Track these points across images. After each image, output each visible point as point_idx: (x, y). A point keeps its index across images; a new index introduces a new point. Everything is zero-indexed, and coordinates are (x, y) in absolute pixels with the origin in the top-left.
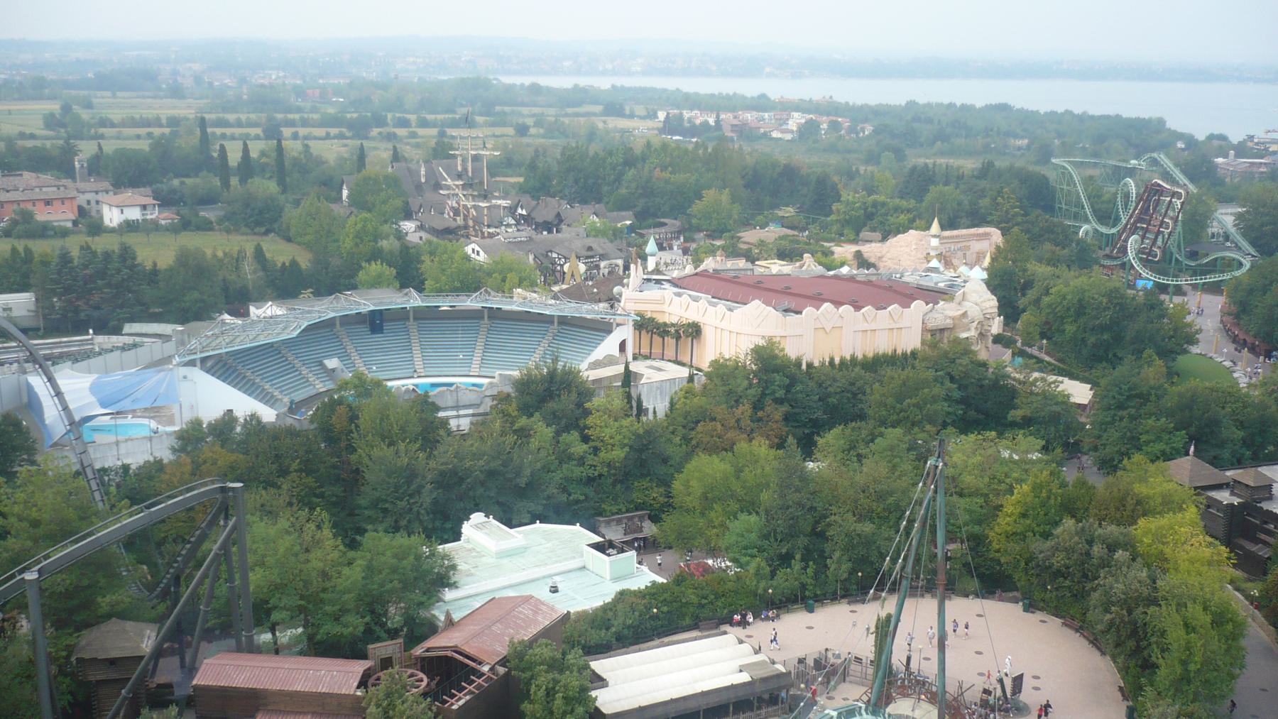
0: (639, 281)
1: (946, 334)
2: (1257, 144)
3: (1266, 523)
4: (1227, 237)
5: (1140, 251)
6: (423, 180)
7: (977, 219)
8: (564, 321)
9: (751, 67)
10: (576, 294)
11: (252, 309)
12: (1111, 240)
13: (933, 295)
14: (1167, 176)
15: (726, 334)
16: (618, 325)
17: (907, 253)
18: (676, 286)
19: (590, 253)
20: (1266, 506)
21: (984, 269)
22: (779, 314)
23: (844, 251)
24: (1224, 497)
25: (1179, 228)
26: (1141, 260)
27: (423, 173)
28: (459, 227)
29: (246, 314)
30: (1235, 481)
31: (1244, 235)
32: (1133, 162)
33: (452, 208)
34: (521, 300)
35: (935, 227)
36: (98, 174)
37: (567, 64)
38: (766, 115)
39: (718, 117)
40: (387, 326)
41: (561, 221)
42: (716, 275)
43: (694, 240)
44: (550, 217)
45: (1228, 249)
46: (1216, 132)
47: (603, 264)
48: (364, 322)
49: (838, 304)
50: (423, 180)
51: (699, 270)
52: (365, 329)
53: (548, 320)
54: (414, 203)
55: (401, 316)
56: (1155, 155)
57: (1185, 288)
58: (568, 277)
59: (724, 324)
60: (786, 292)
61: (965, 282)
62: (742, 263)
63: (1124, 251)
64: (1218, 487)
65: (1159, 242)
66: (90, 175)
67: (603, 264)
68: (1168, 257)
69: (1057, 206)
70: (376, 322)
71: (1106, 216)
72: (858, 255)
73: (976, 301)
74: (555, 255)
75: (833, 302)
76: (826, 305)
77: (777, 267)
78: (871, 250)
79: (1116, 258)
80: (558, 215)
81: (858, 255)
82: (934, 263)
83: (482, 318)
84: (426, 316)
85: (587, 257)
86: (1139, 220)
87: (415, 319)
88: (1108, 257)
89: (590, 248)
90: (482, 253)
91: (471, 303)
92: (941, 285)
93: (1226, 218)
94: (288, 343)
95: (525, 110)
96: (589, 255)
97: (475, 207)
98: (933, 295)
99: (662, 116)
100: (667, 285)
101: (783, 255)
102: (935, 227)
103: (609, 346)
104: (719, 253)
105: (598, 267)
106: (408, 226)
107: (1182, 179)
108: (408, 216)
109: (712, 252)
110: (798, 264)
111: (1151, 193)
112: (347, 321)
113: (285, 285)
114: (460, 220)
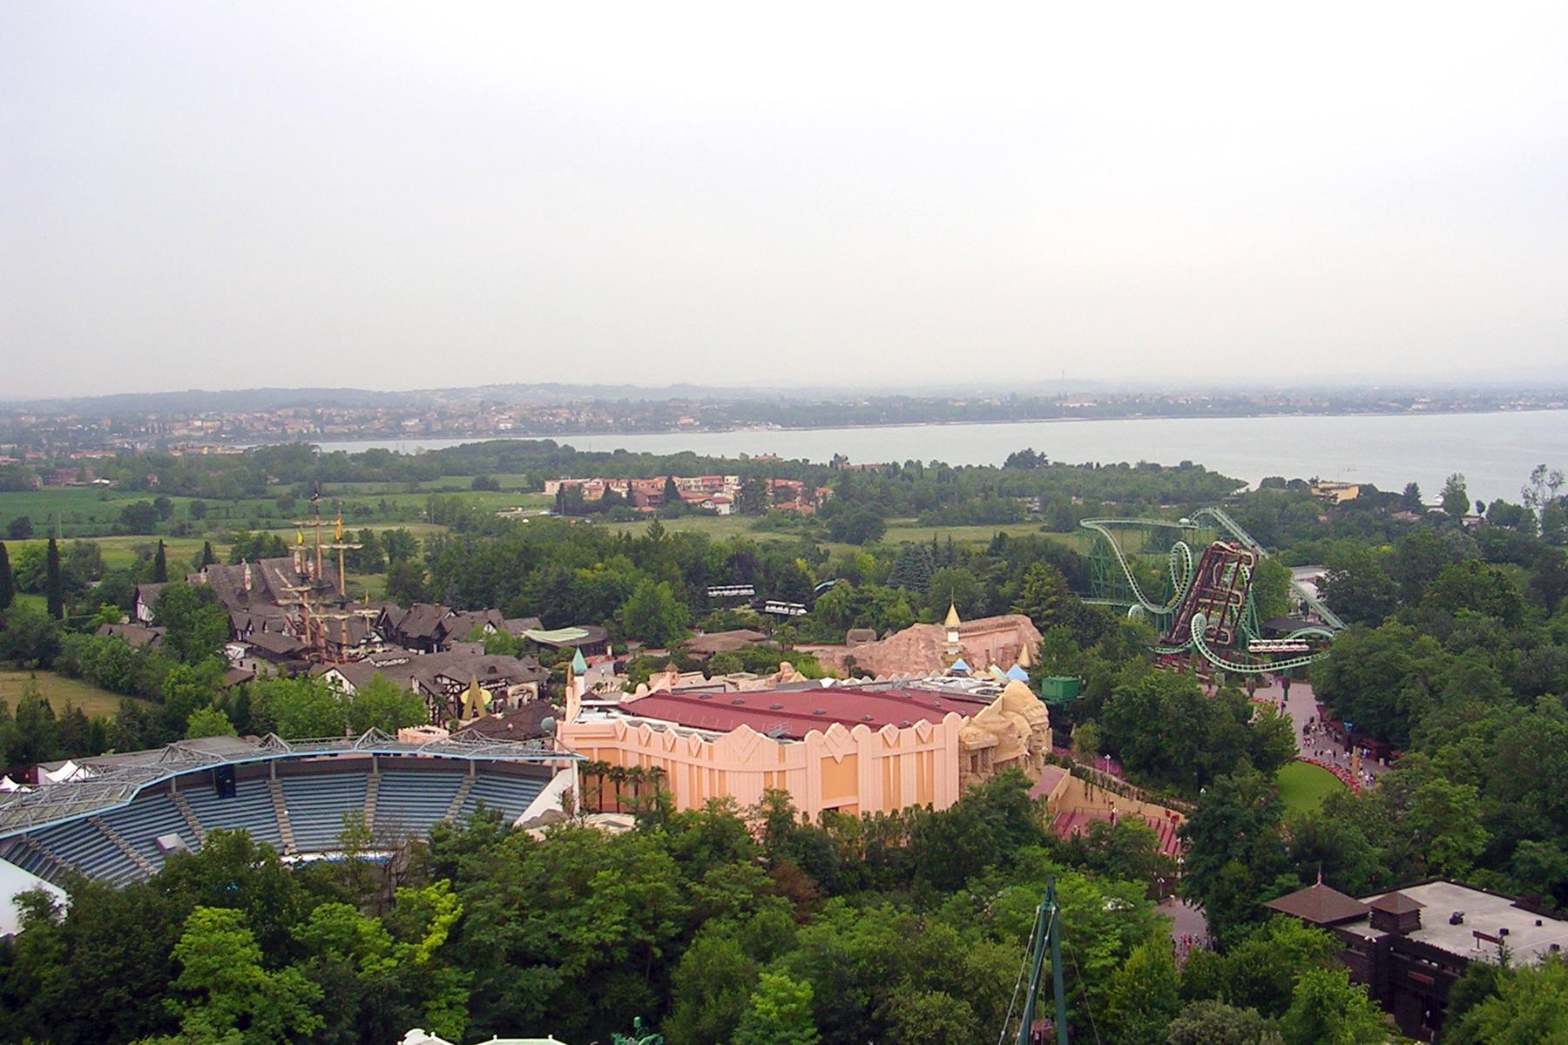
0: (577, 709)
1: (990, 755)
2: (1323, 490)
3: (1419, 958)
4: (1305, 607)
5: (1207, 634)
6: (248, 587)
7: (999, 607)
8: (483, 767)
9: (659, 416)
10: (489, 729)
11: (42, 773)
12: (1165, 622)
13: (969, 704)
14: (1227, 536)
15: (705, 773)
16: (559, 769)
17: (918, 655)
18: (627, 713)
19: (493, 676)
20: (1415, 936)
21: (1024, 668)
22: (775, 742)
23: (829, 656)
24: (1366, 931)
25: (1251, 601)
26: (1207, 643)
27: (248, 577)
28: (306, 650)
29: (33, 781)
30: (1374, 910)
31: (1329, 605)
32: (1184, 520)
33: (293, 623)
34: (425, 739)
35: (953, 618)
36: (1116, 758)
37: (411, 423)
38: (692, 481)
39: (629, 485)
40: (241, 786)
41: (444, 634)
42: (676, 697)
43: (625, 653)
44: (429, 631)
45: (1310, 625)
46: (1149, 461)
47: (510, 690)
48: (209, 783)
49: (849, 724)
50: (248, 587)
51: (653, 691)
52: (209, 792)
53: (459, 766)
54: (240, 620)
55: (259, 771)
56: (1210, 510)
57: (1268, 677)
58: (467, 711)
59: (703, 761)
60: (775, 713)
61: (1002, 686)
62: (697, 679)
63: (1186, 634)
64: (1360, 918)
65: (1227, 622)
66: (1102, 753)
67: (510, 690)
68: (1240, 640)
69: (1093, 581)
70: (224, 781)
71: (1157, 592)
72: (849, 661)
73: (1022, 712)
74: (446, 681)
75: (842, 722)
76: (834, 726)
77: (749, 683)
78: (865, 650)
79: (1177, 645)
80: (440, 626)
81: (849, 661)
82: (960, 664)
83: (370, 770)
84: (289, 768)
85: (489, 682)
86: (1202, 594)
87: (278, 775)
88: (1165, 643)
89: (493, 670)
90: (346, 683)
91: (321, 752)
92: (973, 692)
93: (1305, 585)
94: (112, 817)
95: (363, 487)
96: (492, 678)
97: (328, 621)
98: (969, 704)
99: (552, 488)
100: (615, 713)
101: (754, 666)
102: (953, 618)
103: (547, 800)
104: (670, 666)
105: (504, 694)
106: (236, 650)
107: (1249, 542)
108: (232, 637)
109: (659, 667)
110: (774, 676)
111: (1214, 558)
112: (186, 782)
113: (84, 741)
114: (306, 640)
